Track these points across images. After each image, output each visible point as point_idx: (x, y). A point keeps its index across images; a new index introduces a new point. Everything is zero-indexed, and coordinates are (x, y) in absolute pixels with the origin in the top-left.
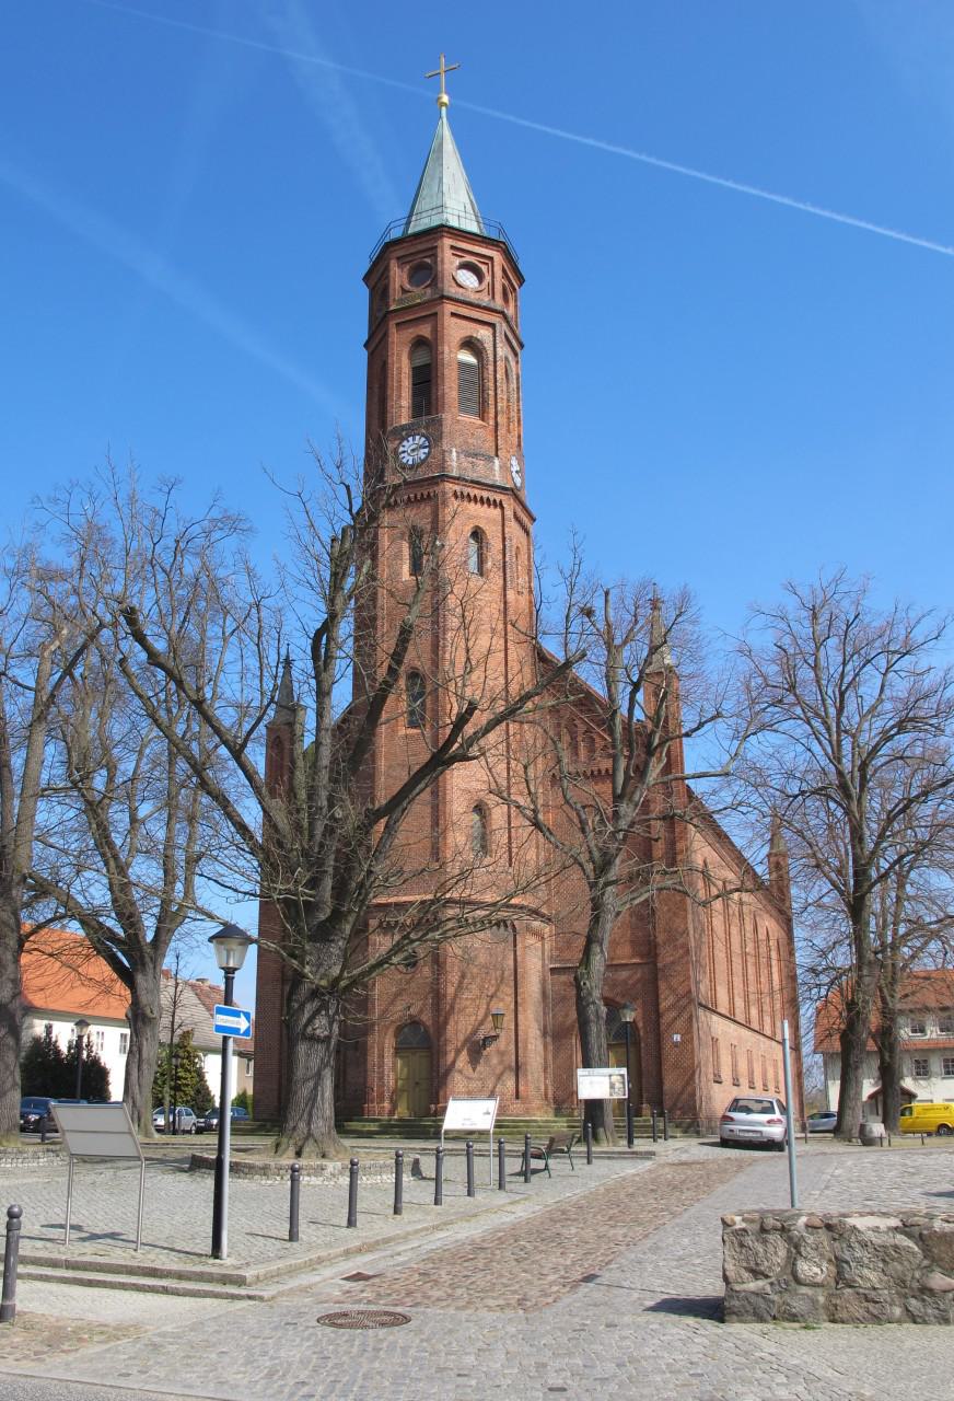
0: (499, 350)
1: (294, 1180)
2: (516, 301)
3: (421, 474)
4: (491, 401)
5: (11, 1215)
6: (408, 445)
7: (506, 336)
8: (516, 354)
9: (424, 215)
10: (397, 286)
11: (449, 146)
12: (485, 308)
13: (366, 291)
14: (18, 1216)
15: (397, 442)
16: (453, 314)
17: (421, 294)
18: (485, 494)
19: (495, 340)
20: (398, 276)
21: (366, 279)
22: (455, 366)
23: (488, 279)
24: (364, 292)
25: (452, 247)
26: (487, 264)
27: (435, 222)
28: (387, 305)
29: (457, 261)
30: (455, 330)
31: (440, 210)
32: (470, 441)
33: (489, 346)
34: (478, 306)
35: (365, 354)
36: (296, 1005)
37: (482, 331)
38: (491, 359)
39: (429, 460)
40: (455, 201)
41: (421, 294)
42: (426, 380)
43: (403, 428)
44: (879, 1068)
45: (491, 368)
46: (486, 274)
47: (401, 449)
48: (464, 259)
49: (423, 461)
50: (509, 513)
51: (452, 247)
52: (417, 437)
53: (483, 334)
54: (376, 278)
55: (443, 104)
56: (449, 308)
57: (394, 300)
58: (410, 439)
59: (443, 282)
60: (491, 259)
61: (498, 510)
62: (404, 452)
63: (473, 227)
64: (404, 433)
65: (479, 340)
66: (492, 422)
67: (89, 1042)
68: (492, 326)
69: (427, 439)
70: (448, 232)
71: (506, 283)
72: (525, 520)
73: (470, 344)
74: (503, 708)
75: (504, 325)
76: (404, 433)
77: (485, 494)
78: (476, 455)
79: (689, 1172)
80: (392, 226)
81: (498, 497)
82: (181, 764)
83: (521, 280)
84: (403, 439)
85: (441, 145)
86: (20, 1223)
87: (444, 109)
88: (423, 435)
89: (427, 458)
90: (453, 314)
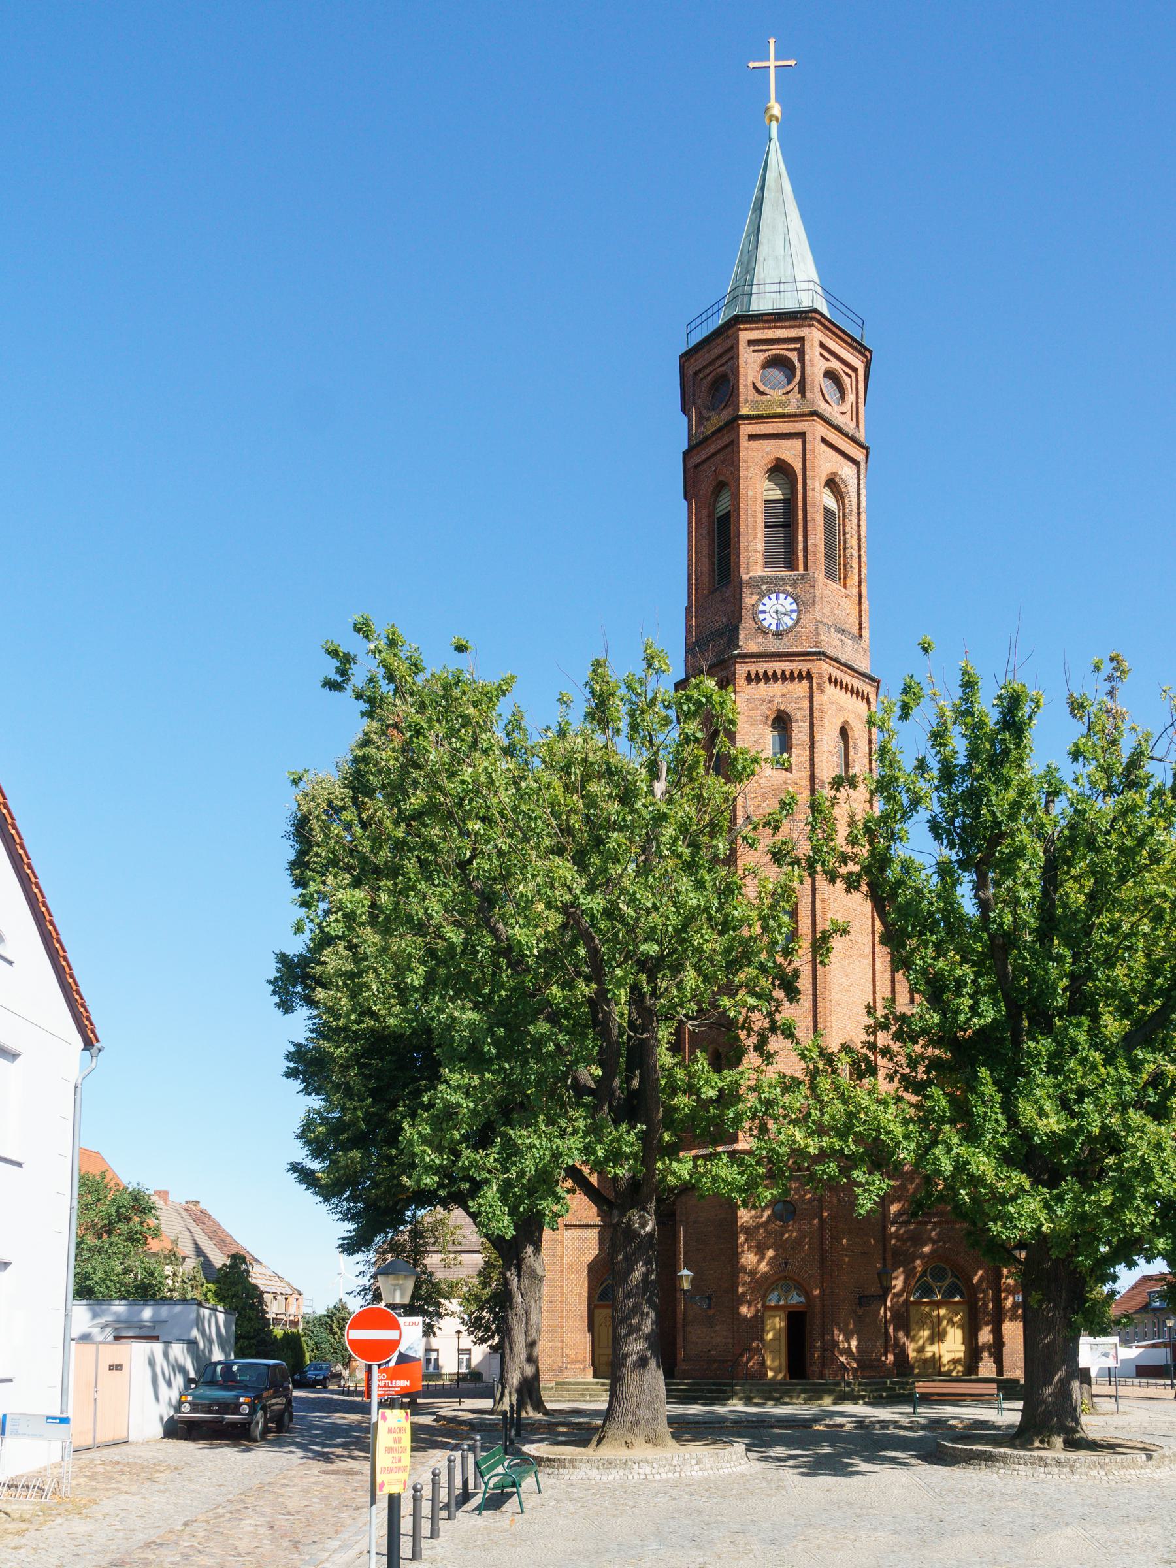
6: (769, 604)
9: (768, 288)
10: (750, 382)
11: (776, 160)
12: (846, 434)
16: (824, 440)
18: (787, 666)
19: (858, 485)
25: (822, 345)
28: (737, 408)
33: (852, 489)
36: (624, 1331)
37: (846, 468)
39: (798, 628)
40: (789, 270)
42: (786, 521)
44: (593, 1268)
47: (761, 608)
49: (790, 630)
51: (822, 345)
52: (782, 596)
53: (847, 472)
55: (771, 118)
56: (818, 429)
57: (747, 401)
58: (773, 596)
60: (855, 370)
61: (805, 683)
62: (764, 612)
65: (843, 481)
66: (855, 591)
67: (539, 1461)
69: (795, 600)
70: (819, 322)
74: (325, 952)
76: (764, 587)
77: (787, 666)
81: (804, 666)
82: (455, 1078)
84: (763, 595)
87: (774, 124)
88: (788, 594)
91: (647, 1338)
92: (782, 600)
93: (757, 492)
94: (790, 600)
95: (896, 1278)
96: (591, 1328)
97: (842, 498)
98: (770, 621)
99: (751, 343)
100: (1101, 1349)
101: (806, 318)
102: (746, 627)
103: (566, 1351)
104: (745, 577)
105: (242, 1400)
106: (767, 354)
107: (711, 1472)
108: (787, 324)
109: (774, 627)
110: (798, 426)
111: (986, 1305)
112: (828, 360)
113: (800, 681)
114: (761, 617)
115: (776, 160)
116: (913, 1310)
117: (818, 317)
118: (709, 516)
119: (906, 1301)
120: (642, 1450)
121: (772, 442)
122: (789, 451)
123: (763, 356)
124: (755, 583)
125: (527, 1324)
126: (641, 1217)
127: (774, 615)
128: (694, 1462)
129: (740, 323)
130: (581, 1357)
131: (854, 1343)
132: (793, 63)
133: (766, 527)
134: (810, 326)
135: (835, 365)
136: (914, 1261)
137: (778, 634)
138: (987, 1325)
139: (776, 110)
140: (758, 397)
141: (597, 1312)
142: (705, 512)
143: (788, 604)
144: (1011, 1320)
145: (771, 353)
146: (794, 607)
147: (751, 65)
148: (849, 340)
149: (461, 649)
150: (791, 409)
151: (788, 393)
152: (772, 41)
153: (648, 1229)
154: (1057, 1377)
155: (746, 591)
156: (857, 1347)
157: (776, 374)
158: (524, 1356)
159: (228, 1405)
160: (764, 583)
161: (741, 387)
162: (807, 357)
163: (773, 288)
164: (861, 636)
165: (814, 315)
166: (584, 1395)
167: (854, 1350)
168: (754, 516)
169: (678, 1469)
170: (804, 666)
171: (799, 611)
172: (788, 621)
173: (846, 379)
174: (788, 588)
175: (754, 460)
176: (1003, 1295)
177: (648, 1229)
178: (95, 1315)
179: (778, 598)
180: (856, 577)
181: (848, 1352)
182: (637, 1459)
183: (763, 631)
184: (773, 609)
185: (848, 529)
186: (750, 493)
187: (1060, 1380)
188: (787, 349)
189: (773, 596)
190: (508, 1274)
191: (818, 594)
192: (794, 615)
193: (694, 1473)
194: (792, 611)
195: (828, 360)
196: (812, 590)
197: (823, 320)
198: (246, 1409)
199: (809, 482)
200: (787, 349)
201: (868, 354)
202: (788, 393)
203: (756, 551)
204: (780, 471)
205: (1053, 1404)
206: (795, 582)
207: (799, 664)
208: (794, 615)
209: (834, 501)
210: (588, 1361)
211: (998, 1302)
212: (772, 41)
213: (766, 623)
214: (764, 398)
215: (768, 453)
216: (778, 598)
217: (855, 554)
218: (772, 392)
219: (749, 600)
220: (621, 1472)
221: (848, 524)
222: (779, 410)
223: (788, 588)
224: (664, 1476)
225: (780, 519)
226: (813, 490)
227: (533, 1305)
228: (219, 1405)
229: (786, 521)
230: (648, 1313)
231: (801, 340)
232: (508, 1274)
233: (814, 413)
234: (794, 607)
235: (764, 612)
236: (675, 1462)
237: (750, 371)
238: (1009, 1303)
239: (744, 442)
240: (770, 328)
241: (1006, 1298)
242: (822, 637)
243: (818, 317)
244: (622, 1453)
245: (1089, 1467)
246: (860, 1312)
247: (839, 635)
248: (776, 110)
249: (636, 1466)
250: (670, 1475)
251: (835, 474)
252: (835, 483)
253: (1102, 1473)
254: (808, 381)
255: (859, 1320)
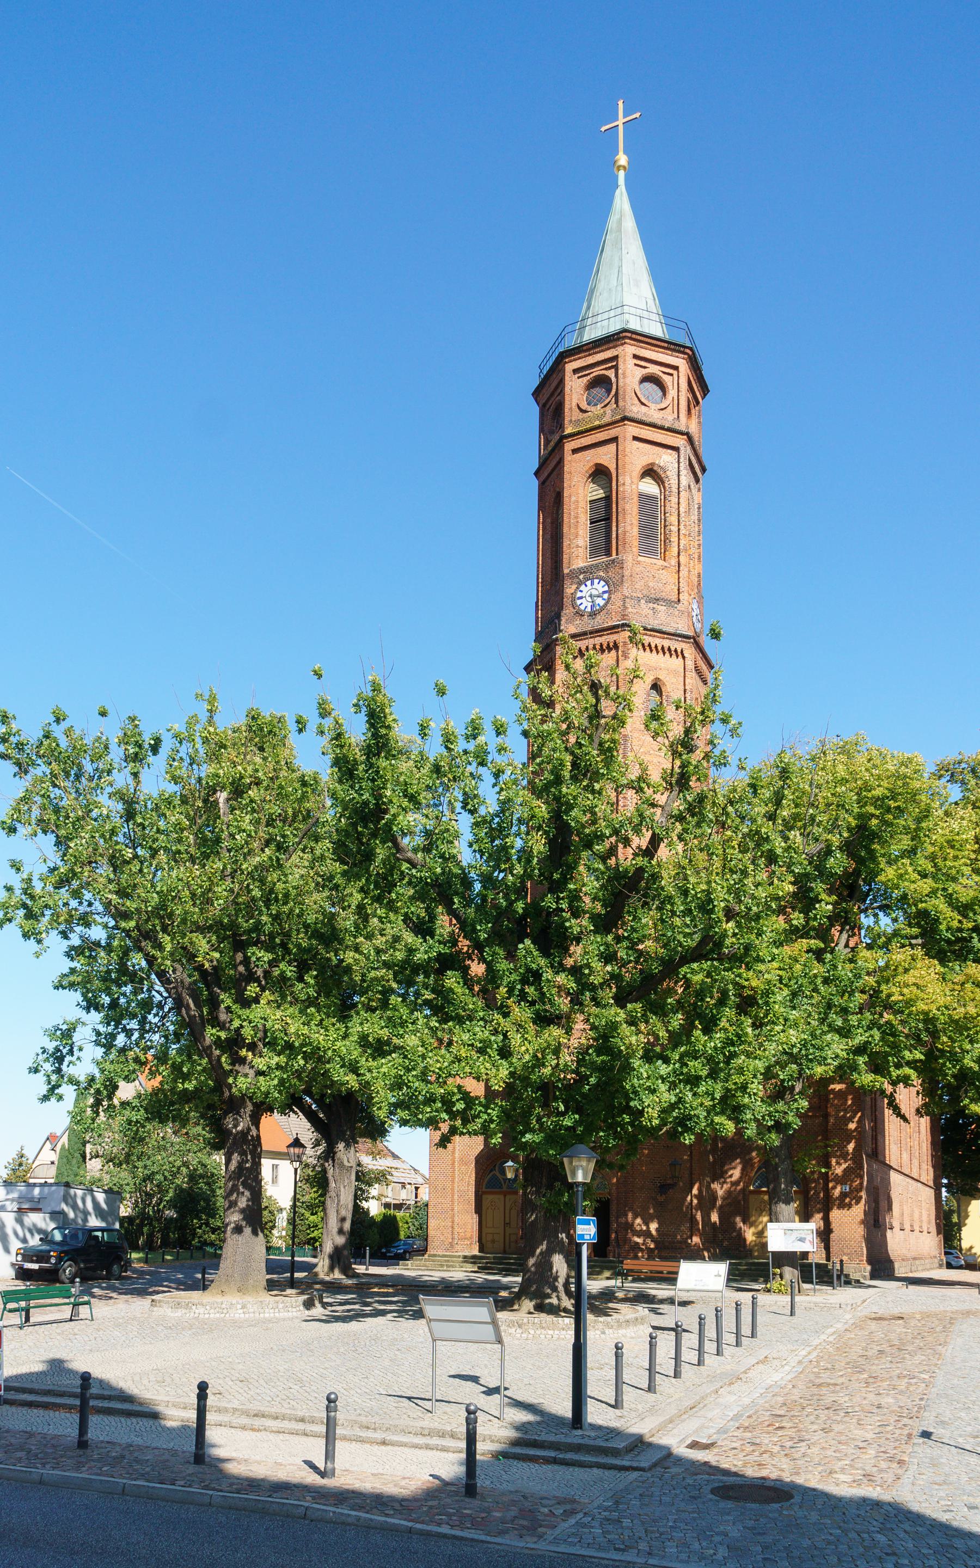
0: (683, 478)
1: (672, 1329)
2: (699, 417)
3: (601, 621)
4: (674, 539)
5: (617, 1347)
6: (585, 590)
7: (690, 460)
8: (697, 481)
9: (600, 318)
10: (574, 404)
11: (622, 201)
13: (536, 409)
14: (655, 1338)
15: (574, 587)
16: (635, 438)
17: (601, 412)
18: (666, 643)
20: (575, 389)
21: (536, 394)
22: (636, 499)
23: (672, 393)
24: (534, 410)
26: (671, 375)
27: (614, 327)
28: (561, 426)
29: (640, 373)
30: (638, 456)
31: (619, 311)
32: (651, 584)
33: (672, 474)
34: (662, 428)
35: (535, 483)
38: (675, 490)
39: (609, 606)
40: (626, 292)
41: (601, 412)
42: (604, 516)
43: (582, 571)
45: (674, 500)
46: (671, 387)
47: (579, 594)
48: (647, 371)
49: (602, 608)
50: (690, 664)
51: (635, 357)
52: (596, 581)
53: (666, 459)
54: (549, 395)
55: (619, 168)
56: (632, 430)
57: (571, 421)
58: (589, 583)
59: (624, 401)
60: (676, 368)
62: (581, 598)
63: (656, 329)
64: (581, 577)
65: (662, 468)
66: (674, 562)
68: (676, 449)
69: (607, 583)
70: (631, 338)
71: (690, 396)
72: (704, 667)
73: (650, 472)
75: (689, 448)
76: (581, 577)
77: (666, 643)
78: (657, 600)
79: (960, 1440)
80: (567, 330)
81: (611, 638)
83: (705, 390)
85: (620, 222)
86: (336, 1406)
88: (601, 579)
89: (606, 604)
90: (635, 438)
91: (242, 1211)
92: (596, 585)
93: (580, 494)
94: (602, 583)
95: (735, 1168)
96: (479, 1209)
97: (663, 483)
98: (585, 605)
99: (575, 371)
100: (796, 1235)
101: (618, 339)
102: (567, 612)
103: (456, 1229)
104: (566, 571)
105: (52, 1253)
106: (589, 377)
107: (252, 1315)
108: (603, 348)
109: (589, 609)
110: (612, 433)
111: (817, 1194)
112: (645, 367)
113: (609, 652)
114: (579, 602)
115: (622, 201)
116: (752, 1198)
117: (629, 335)
118: (552, 523)
119: (743, 1190)
120: (233, 1299)
121: (592, 451)
122: (605, 456)
123: (585, 380)
124: (574, 574)
125: (338, 1204)
126: (235, 1119)
127: (589, 599)
128: (239, 1306)
129: (566, 357)
130: (469, 1235)
131: (653, 1226)
132: (637, 115)
133: (591, 523)
134: (622, 344)
135: (654, 369)
136: (750, 1153)
137: (593, 614)
138: (818, 1213)
139: (623, 159)
140: (581, 416)
141: (487, 1199)
142: (549, 520)
143: (600, 587)
144: (839, 1208)
145: (594, 374)
146: (606, 588)
147: (603, 129)
148: (666, 345)
149: (103, 714)
150: (607, 419)
151: (605, 406)
152: (620, 103)
153: (239, 1128)
154: (538, 1251)
155: (567, 582)
156: (657, 1230)
157: (599, 391)
158: (335, 1230)
159: (43, 1257)
160: (581, 573)
161: (566, 410)
162: (620, 371)
163: (606, 316)
164: (679, 600)
165: (624, 334)
166: (442, 1266)
167: (654, 1232)
168: (576, 517)
169: (225, 1311)
170: (611, 638)
171: (609, 592)
172: (600, 602)
173: (665, 377)
174: (601, 574)
175: (576, 468)
176: (831, 1185)
177: (239, 1128)
178: (8, 1193)
179: (592, 584)
180: (676, 549)
181: (647, 1234)
182: (196, 1301)
183: (580, 614)
184: (588, 594)
185: (668, 508)
186: (573, 499)
187: (541, 1253)
188: (606, 369)
189: (589, 583)
190: (327, 1164)
191: (627, 573)
192: (606, 596)
193: (237, 1315)
194: (604, 592)
195: (645, 367)
196: (620, 571)
197: (634, 336)
198: (53, 1261)
199: (620, 478)
200: (606, 369)
201: (688, 351)
202: (605, 406)
203: (578, 546)
204: (600, 474)
205: (535, 1273)
206: (607, 567)
207: (612, 634)
208: (606, 596)
209: (656, 487)
210: (476, 1238)
211: (827, 1191)
212: (620, 103)
213: (582, 607)
214: (586, 415)
215: (588, 461)
216: (592, 584)
217: (674, 529)
218: (593, 409)
219: (569, 589)
220: (184, 1311)
221: (668, 504)
222: (597, 423)
223: (601, 574)
224: (212, 1316)
225: (602, 514)
226: (624, 484)
227: (342, 1189)
228: (37, 1256)
229: (604, 516)
230: (243, 1193)
231: (616, 358)
232: (327, 1164)
233: (625, 418)
234: (606, 588)
235: (581, 598)
236: (224, 1306)
237: (574, 397)
238: (837, 1192)
239: (568, 457)
240: (590, 355)
241: (834, 1188)
242: (630, 610)
243: (629, 335)
244: (219, 1299)
245: (509, 1326)
246: (661, 1199)
247: (651, 605)
248: (623, 159)
249: (194, 1307)
250: (218, 1315)
251: (653, 464)
252: (655, 472)
253: (519, 1331)
254: (621, 392)
255: (660, 1206)
